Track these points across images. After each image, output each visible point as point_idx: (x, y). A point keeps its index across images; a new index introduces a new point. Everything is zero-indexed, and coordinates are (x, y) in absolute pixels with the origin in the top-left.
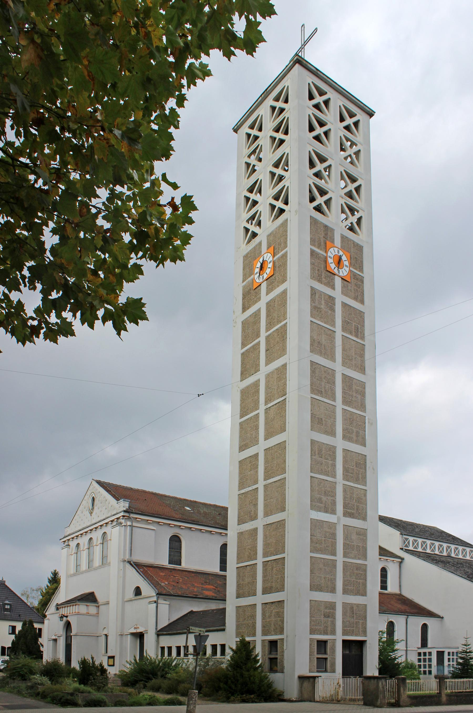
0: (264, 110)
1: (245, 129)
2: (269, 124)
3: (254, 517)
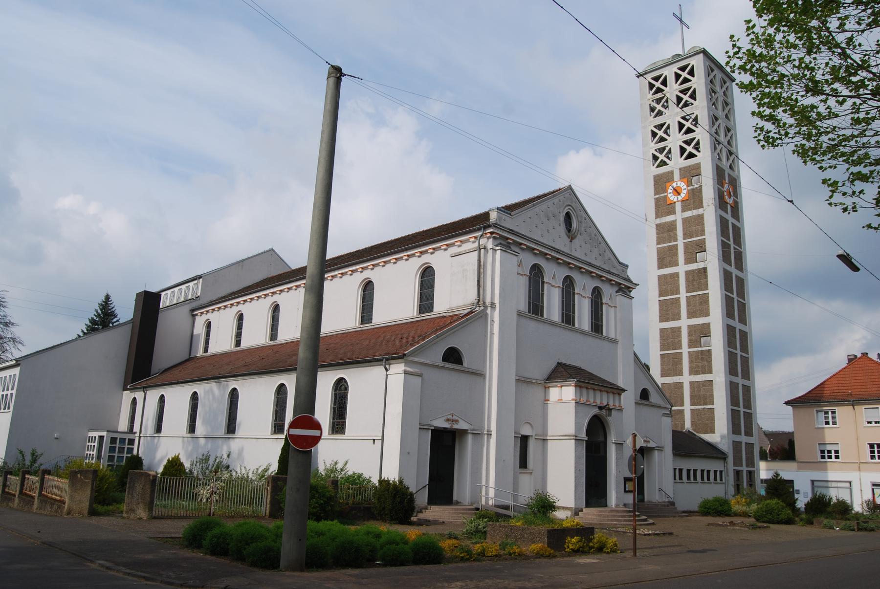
0: (669, 72)
1: (649, 77)
2: (672, 90)
3: (677, 317)
